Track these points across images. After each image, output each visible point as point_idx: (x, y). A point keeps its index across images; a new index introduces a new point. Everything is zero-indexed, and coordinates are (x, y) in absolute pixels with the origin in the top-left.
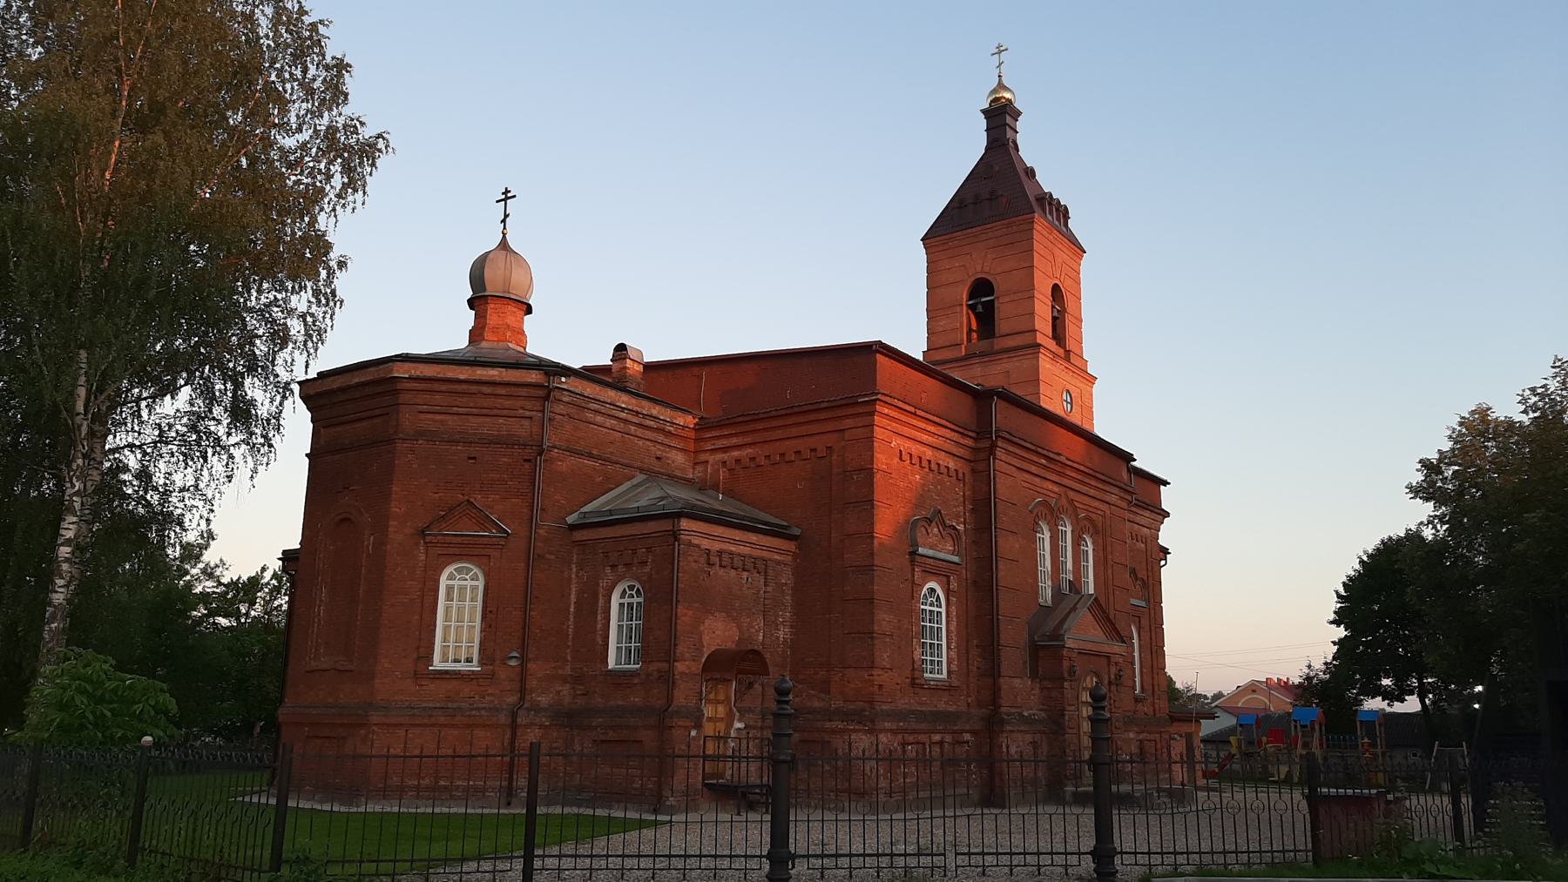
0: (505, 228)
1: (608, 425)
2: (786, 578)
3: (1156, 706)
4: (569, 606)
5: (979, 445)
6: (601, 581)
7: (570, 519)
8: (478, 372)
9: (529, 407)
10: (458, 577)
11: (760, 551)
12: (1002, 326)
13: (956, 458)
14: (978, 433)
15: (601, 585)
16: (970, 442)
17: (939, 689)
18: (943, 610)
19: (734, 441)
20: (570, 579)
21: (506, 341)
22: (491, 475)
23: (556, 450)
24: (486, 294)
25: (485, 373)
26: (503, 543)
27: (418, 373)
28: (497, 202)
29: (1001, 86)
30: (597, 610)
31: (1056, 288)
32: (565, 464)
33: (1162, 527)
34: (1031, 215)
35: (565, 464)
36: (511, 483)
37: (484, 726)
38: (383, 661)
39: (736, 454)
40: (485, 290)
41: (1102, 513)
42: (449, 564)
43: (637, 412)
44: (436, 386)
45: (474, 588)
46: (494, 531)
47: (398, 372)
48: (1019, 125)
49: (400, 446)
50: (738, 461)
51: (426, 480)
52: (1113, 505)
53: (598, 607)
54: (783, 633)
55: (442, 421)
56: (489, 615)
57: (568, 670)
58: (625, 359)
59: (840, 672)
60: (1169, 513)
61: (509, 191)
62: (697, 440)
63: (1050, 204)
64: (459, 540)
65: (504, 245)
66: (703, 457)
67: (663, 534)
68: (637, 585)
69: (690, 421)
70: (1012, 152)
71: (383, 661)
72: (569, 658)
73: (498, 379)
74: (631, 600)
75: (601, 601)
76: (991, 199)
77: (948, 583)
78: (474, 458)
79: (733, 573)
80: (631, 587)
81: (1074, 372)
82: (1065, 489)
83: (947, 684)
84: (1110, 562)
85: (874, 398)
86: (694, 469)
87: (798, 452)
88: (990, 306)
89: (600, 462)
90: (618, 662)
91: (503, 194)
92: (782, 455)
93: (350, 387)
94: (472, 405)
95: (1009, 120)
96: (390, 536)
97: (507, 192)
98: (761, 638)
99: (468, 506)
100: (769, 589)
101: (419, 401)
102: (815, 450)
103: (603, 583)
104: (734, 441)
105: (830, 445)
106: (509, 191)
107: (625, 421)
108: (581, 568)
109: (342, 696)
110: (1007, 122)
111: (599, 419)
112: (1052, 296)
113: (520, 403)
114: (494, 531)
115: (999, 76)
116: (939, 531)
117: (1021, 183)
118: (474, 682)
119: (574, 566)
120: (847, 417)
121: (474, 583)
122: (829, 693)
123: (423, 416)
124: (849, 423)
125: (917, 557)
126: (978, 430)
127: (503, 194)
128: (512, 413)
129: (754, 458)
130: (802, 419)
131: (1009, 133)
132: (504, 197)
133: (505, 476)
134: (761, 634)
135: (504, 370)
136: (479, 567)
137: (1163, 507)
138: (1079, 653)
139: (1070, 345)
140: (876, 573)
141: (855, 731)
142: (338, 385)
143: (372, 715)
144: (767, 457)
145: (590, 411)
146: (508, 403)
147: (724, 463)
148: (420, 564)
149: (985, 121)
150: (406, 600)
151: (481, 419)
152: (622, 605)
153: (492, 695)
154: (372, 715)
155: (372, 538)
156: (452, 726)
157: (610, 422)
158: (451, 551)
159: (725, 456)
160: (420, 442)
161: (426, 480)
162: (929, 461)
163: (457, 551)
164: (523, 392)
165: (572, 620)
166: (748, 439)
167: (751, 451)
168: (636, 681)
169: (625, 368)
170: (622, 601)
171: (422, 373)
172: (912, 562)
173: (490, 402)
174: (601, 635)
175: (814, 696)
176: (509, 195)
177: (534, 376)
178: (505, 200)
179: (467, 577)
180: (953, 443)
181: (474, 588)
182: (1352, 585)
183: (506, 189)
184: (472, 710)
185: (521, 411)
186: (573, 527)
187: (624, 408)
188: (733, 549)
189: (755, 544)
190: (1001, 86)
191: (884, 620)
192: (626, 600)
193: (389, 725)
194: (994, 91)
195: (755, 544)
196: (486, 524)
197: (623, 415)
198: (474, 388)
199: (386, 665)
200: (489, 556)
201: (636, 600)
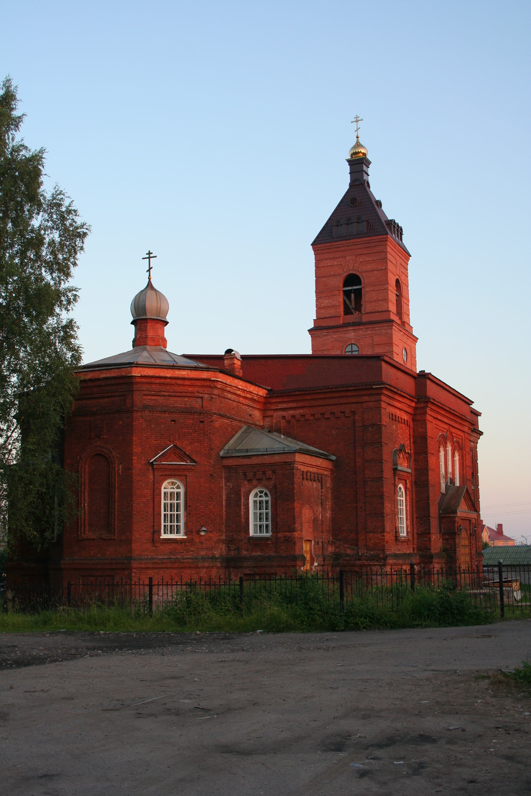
0: (150, 275)
1: (232, 399)
2: (329, 484)
3: (477, 545)
4: (223, 502)
5: (419, 406)
6: (242, 488)
7: (222, 453)
8: (177, 373)
9: (201, 392)
10: (170, 487)
11: (320, 470)
12: (367, 307)
13: (407, 414)
14: (418, 399)
15: (242, 490)
16: (413, 404)
17: (406, 542)
18: (404, 499)
19: (292, 405)
20: (222, 487)
21: (159, 345)
22: (183, 430)
23: (215, 416)
24: (148, 317)
25: (180, 373)
26: (193, 468)
27: (145, 374)
28: (143, 259)
29: (358, 145)
30: (241, 504)
31: (397, 281)
32: (219, 422)
33: (479, 441)
34: (385, 236)
35: (219, 422)
36: (195, 435)
37: (190, 567)
38: (135, 534)
39: (292, 412)
40: (145, 314)
41: (461, 438)
42: (166, 480)
43: (245, 390)
44: (153, 380)
45: (267, 502)
46: (188, 462)
47: (135, 373)
48: (370, 170)
49: (136, 415)
50: (293, 416)
51: (150, 433)
52: (466, 433)
53: (241, 503)
54: (328, 514)
55: (155, 400)
56: (188, 508)
57: (224, 537)
58: (234, 358)
59: (364, 534)
60: (482, 433)
61: (152, 253)
62: (265, 403)
63: (394, 227)
64: (171, 466)
65: (150, 285)
66: (269, 413)
67: (283, 463)
68: (265, 491)
69: (262, 392)
70: (367, 188)
71: (135, 534)
72: (224, 530)
73: (187, 377)
74: (261, 499)
75: (243, 500)
76: (358, 222)
77: (406, 484)
78: (174, 421)
79: (310, 483)
80: (261, 492)
81: (408, 336)
82: (450, 426)
83: (407, 539)
84: (465, 466)
85: (383, 386)
86: (264, 420)
87: (332, 413)
88: (358, 293)
89: (230, 420)
90: (255, 532)
91: (147, 254)
92: (323, 414)
93: (99, 380)
94: (171, 390)
95: (365, 168)
96: (134, 465)
97: (149, 253)
98: (321, 517)
99: (175, 449)
100: (323, 490)
101: (144, 388)
102: (344, 412)
103: (243, 490)
104: (292, 405)
105: (353, 410)
106: (152, 253)
107: (239, 396)
108: (228, 480)
109: (108, 553)
110: (364, 169)
111: (229, 396)
112: (396, 286)
113: (196, 389)
114: (188, 462)
115: (357, 137)
116: (403, 456)
117: (375, 209)
118: (183, 544)
119: (223, 480)
120: (365, 395)
121: (178, 490)
122: (357, 545)
123: (145, 397)
124: (366, 398)
125: (397, 471)
126: (417, 398)
127: (147, 254)
128: (192, 395)
129: (304, 415)
130: (337, 395)
131: (365, 176)
132: (148, 256)
133: (191, 431)
134: (321, 515)
135: (190, 371)
136: (181, 481)
137: (480, 429)
138: (461, 519)
139: (405, 319)
140: (384, 482)
141: (375, 565)
142: (89, 378)
143: (133, 563)
144: (313, 415)
145: (226, 392)
146: (190, 389)
147: (284, 417)
148: (151, 481)
149: (349, 167)
150: (145, 501)
151: (176, 399)
152: (255, 502)
153: (192, 551)
154: (133, 563)
155: (121, 466)
156: (174, 568)
157: (233, 397)
158: (166, 473)
159: (285, 414)
160: (146, 412)
161: (150, 433)
162: (398, 417)
163: (170, 473)
164: (199, 383)
165: (224, 509)
166: (301, 404)
167: (301, 411)
168: (270, 542)
169: (234, 364)
170: (255, 499)
171: (147, 373)
172: (395, 474)
173: (181, 389)
174: (244, 517)
175: (348, 547)
176: (151, 255)
177: (205, 374)
178: (149, 258)
179: (174, 487)
180: (407, 406)
181: (267, 502)
182: (133, 341)
183: (149, 251)
184: (184, 559)
185: (197, 394)
186: (223, 458)
187: (240, 389)
188: (311, 470)
189: (319, 467)
190: (358, 145)
191: (387, 505)
192: (258, 499)
193: (142, 568)
194: (354, 147)
195: (319, 467)
196: (184, 458)
197: (239, 392)
198: (173, 381)
199: (137, 536)
200: (186, 475)
201: (264, 499)
